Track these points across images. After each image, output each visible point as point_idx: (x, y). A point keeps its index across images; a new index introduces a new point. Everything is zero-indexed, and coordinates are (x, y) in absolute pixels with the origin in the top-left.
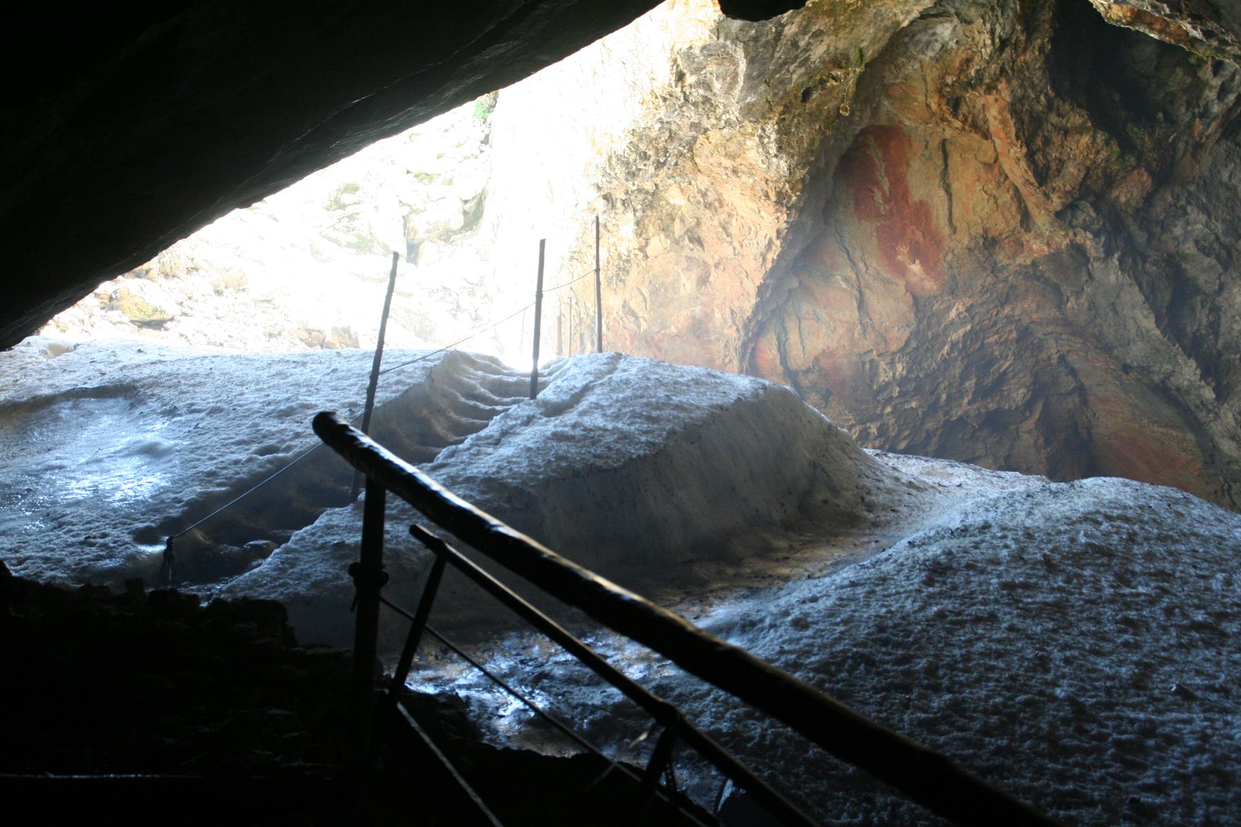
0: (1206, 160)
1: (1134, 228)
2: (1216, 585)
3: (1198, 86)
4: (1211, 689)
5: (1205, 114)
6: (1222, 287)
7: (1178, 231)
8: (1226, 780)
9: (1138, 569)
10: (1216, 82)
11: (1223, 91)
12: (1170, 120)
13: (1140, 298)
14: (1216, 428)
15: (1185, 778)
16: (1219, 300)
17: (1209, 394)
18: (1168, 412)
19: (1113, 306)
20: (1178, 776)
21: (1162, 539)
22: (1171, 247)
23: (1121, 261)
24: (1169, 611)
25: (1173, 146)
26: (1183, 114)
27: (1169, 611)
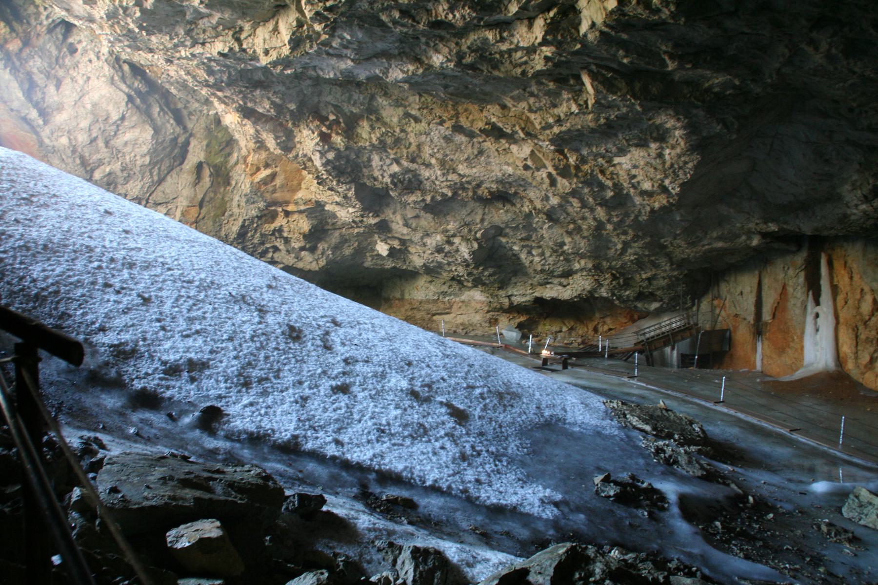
0: (41, 41)
1: (15, 60)
2: (31, 185)
3: (38, 14)
4: (26, 219)
5: (41, 24)
6: (46, 86)
7: (31, 63)
8: (28, 249)
9: (4, 178)
10: (45, 13)
11: (48, 17)
12: (28, 23)
13: (17, 85)
14: (43, 134)
15: (14, 249)
16: (45, 90)
17: (41, 122)
18: (27, 127)
19: (7, 87)
20: (12, 248)
21: (14, 169)
22: (29, 69)
23: (10, 71)
24: (14, 193)
25: (30, 33)
26: (33, 22)
27: (14, 193)
